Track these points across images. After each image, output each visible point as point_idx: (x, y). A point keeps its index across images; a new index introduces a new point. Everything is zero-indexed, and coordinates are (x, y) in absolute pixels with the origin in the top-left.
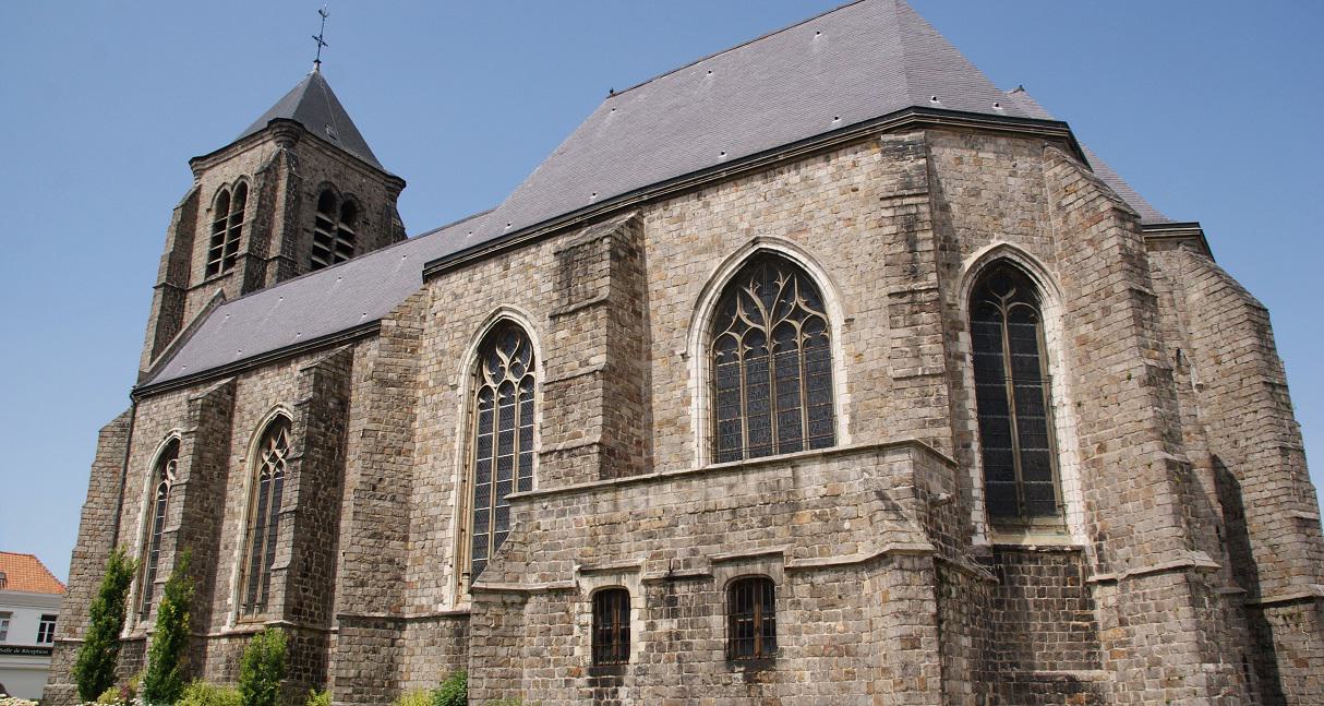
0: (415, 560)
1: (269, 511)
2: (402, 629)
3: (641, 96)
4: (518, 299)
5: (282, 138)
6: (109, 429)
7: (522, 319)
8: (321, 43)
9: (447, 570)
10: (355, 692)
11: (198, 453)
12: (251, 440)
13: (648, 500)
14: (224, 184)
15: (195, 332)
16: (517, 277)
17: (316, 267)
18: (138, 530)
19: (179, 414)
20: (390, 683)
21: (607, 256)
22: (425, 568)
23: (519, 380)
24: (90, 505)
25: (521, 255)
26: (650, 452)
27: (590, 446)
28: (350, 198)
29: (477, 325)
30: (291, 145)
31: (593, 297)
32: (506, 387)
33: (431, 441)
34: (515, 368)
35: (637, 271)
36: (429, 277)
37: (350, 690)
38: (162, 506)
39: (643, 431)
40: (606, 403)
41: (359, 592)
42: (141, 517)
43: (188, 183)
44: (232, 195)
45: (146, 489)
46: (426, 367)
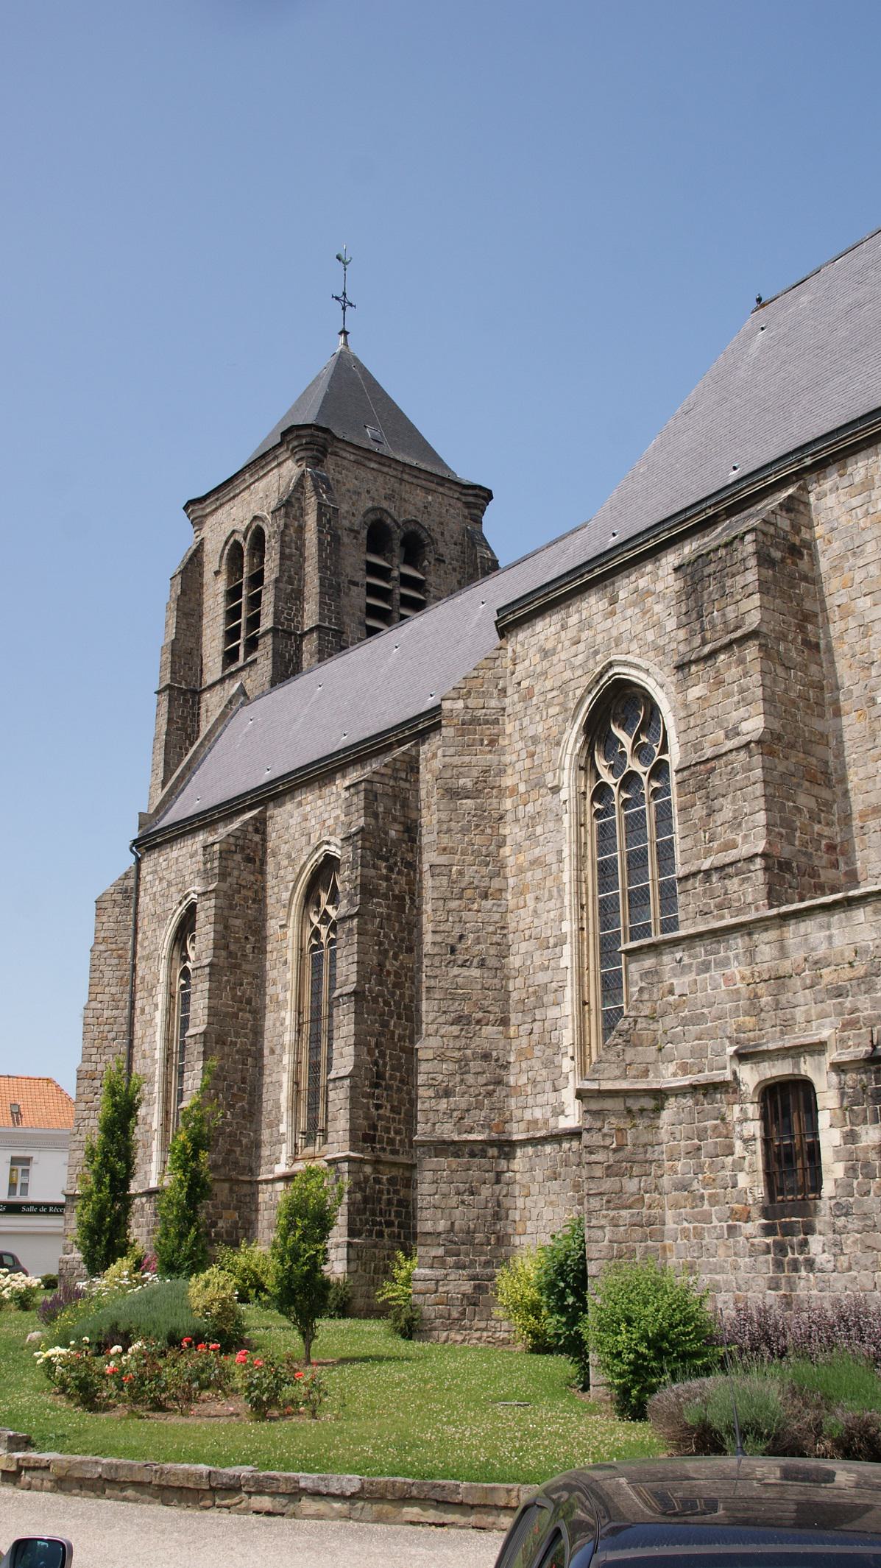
0: (520, 1053)
1: (325, 996)
2: (509, 1156)
3: (804, 298)
4: (634, 646)
5: (302, 454)
6: (108, 897)
7: (643, 675)
8: (346, 304)
9: (567, 1064)
10: (448, 1253)
11: (222, 920)
12: (292, 895)
13: (830, 937)
14: (234, 532)
15: (210, 749)
16: (629, 612)
17: (372, 632)
18: (158, 1034)
19: (195, 867)
20: (498, 1238)
21: (752, 562)
22: (536, 1064)
23: (648, 769)
24: (93, 1005)
25: (633, 578)
26: (850, 861)
27: (751, 859)
28: (412, 527)
29: (579, 692)
30: (317, 462)
31: (737, 628)
32: (630, 781)
33: (530, 874)
34: (640, 751)
35: (805, 578)
36: (505, 630)
37: (440, 1251)
38: (186, 999)
39: (837, 828)
40: (770, 790)
41: (443, 1104)
42: (159, 1017)
43: (185, 540)
44: (246, 546)
45: (162, 976)
46: (512, 764)
